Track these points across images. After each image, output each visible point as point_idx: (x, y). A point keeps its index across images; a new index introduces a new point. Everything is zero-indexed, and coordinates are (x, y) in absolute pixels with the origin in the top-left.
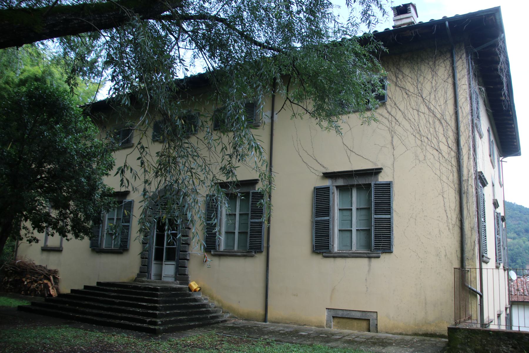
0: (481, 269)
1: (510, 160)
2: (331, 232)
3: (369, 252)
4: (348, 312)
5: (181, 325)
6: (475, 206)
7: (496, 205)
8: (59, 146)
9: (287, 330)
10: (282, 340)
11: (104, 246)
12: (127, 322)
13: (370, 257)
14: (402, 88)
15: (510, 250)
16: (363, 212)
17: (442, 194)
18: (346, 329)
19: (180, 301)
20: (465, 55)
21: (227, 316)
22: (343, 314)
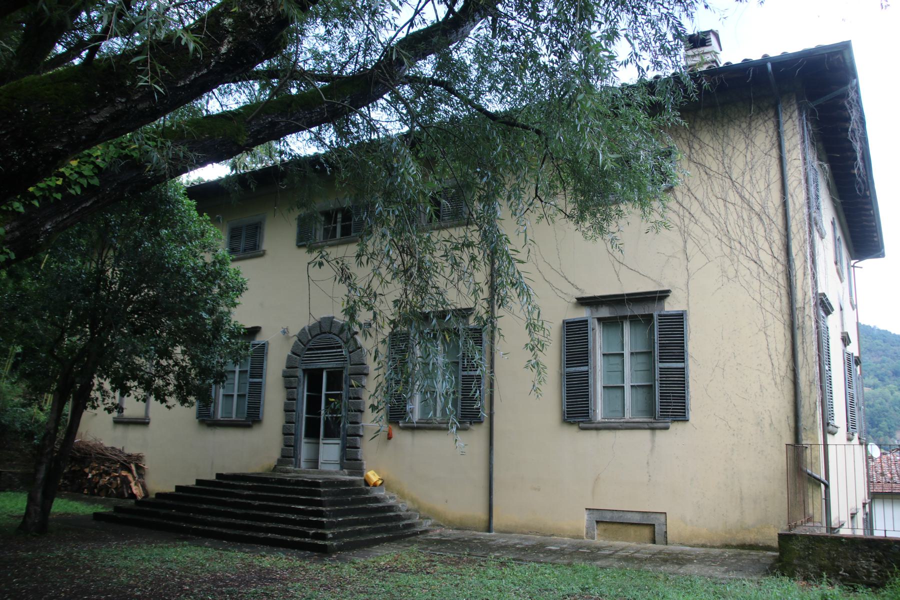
0: (826, 445)
1: (868, 265)
2: (591, 389)
3: (652, 420)
4: (621, 514)
5: (363, 539)
6: (815, 347)
7: (846, 340)
8: (168, 263)
9: (527, 543)
10: (522, 558)
11: (219, 416)
12: (278, 536)
13: (653, 429)
14: (699, 164)
15: (868, 406)
16: (641, 359)
17: (764, 329)
18: (617, 540)
19: (354, 502)
20: (796, 113)
21: (426, 524)
22: (612, 517)
